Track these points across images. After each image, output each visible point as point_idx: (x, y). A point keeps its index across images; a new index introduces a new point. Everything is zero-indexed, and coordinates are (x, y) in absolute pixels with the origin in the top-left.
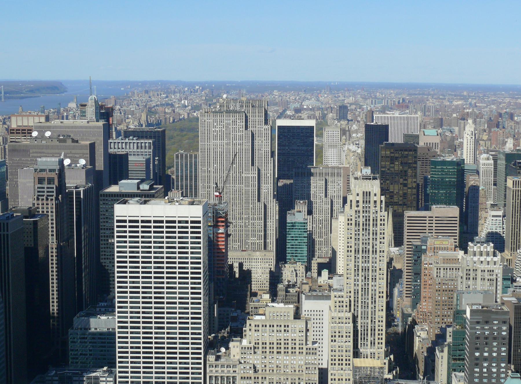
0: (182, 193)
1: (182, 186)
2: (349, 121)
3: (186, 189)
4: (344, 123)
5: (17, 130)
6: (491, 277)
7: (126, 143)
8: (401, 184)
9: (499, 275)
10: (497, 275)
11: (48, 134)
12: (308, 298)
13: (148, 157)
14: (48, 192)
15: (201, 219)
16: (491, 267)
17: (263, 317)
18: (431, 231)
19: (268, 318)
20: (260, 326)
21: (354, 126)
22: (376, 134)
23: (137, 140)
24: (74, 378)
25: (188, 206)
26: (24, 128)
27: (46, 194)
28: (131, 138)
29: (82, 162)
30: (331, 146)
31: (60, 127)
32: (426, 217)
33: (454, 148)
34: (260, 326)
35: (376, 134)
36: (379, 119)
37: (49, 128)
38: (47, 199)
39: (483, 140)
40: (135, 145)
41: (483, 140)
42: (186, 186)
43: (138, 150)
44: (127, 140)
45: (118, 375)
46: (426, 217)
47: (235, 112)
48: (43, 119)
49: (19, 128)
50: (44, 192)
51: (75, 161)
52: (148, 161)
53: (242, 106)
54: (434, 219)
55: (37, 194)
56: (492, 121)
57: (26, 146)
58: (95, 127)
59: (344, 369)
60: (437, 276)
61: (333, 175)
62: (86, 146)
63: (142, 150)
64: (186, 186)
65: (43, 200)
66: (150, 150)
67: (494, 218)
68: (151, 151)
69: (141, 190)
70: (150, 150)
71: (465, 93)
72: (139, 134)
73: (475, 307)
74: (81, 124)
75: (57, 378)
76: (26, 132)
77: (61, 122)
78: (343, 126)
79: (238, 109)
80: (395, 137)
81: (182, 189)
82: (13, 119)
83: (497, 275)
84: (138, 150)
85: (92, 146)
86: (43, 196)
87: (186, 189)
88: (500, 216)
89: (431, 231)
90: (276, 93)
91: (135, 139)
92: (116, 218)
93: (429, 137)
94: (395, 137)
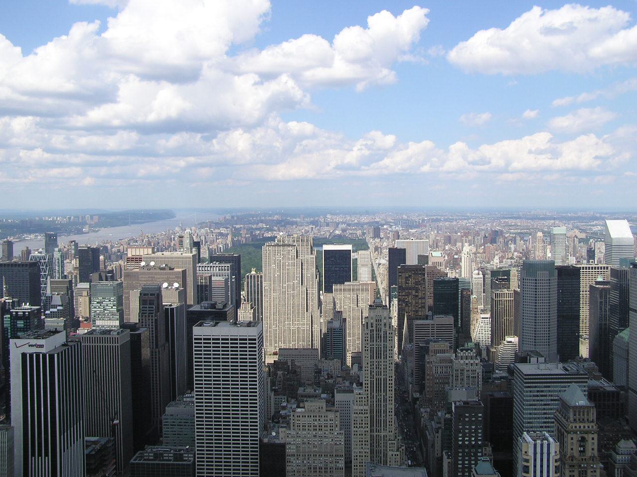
0: (251, 305)
1: (251, 299)
2: (381, 238)
3: (255, 301)
4: (377, 240)
5: (132, 258)
6: (474, 375)
7: (211, 267)
8: (414, 295)
9: (480, 374)
10: (478, 374)
11: (152, 264)
12: (338, 392)
13: (227, 277)
14: (149, 310)
15: (257, 338)
16: (474, 367)
17: (303, 410)
18: (433, 335)
19: (307, 410)
20: (301, 416)
21: (385, 243)
22: (397, 256)
23: (219, 264)
24: (165, 455)
25: (246, 328)
26: (137, 257)
27: (148, 312)
28: (214, 262)
29: (176, 285)
30: (363, 265)
31: (162, 258)
32: (429, 325)
33: (455, 263)
34: (301, 416)
35: (397, 256)
36: (398, 244)
37: (153, 259)
38: (149, 316)
39: (480, 253)
40: (217, 268)
41: (480, 253)
42: (255, 299)
43: (220, 272)
44: (211, 264)
45: (197, 452)
46: (429, 325)
47: (289, 245)
48: (150, 251)
49: (133, 257)
50: (146, 310)
51: (171, 284)
52: (226, 281)
53: (294, 241)
54: (435, 326)
55: (141, 312)
56: (487, 237)
57: (137, 273)
58: (186, 258)
59: (364, 448)
60: (436, 373)
61: (363, 290)
62: (179, 272)
63: (225, 272)
64: (255, 299)
65: (146, 316)
66: (228, 272)
67: (483, 320)
68: (229, 272)
69: (218, 309)
70: (228, 272)
71: (468, 214)
72: (221, 259)
73: (458, 404)
74: (177, 256)
75: (152, 455)
76: (138, 259)
77: (162, 254)
78: (377, 244)
79: (291, 243)
80: (412, 260)
81: (251, 301)
82: (129, 250)
83: (478, 374)
84: (220, 272)
85: (184, 272)
86: (146, 313)
87: (255, 301)
88: (488, 318)
89: (433, 335)
90: (329, 216)
91: (217, 263)
92: (194, 337)
93: (436, 256)
94: (412, 260)
